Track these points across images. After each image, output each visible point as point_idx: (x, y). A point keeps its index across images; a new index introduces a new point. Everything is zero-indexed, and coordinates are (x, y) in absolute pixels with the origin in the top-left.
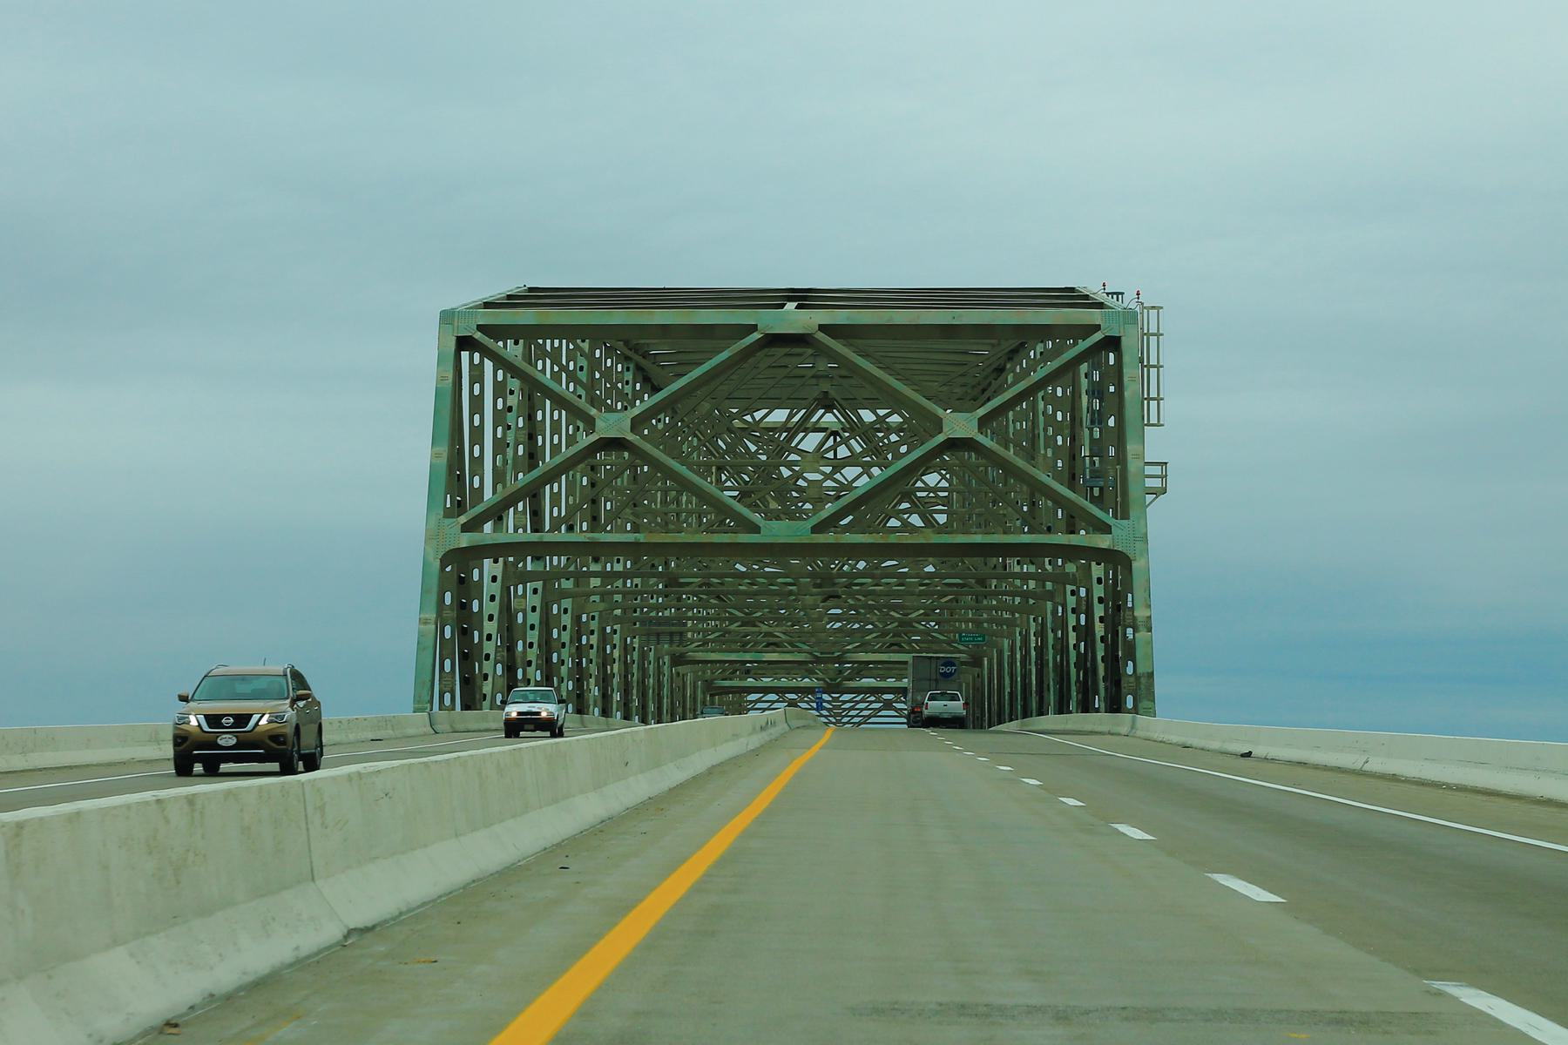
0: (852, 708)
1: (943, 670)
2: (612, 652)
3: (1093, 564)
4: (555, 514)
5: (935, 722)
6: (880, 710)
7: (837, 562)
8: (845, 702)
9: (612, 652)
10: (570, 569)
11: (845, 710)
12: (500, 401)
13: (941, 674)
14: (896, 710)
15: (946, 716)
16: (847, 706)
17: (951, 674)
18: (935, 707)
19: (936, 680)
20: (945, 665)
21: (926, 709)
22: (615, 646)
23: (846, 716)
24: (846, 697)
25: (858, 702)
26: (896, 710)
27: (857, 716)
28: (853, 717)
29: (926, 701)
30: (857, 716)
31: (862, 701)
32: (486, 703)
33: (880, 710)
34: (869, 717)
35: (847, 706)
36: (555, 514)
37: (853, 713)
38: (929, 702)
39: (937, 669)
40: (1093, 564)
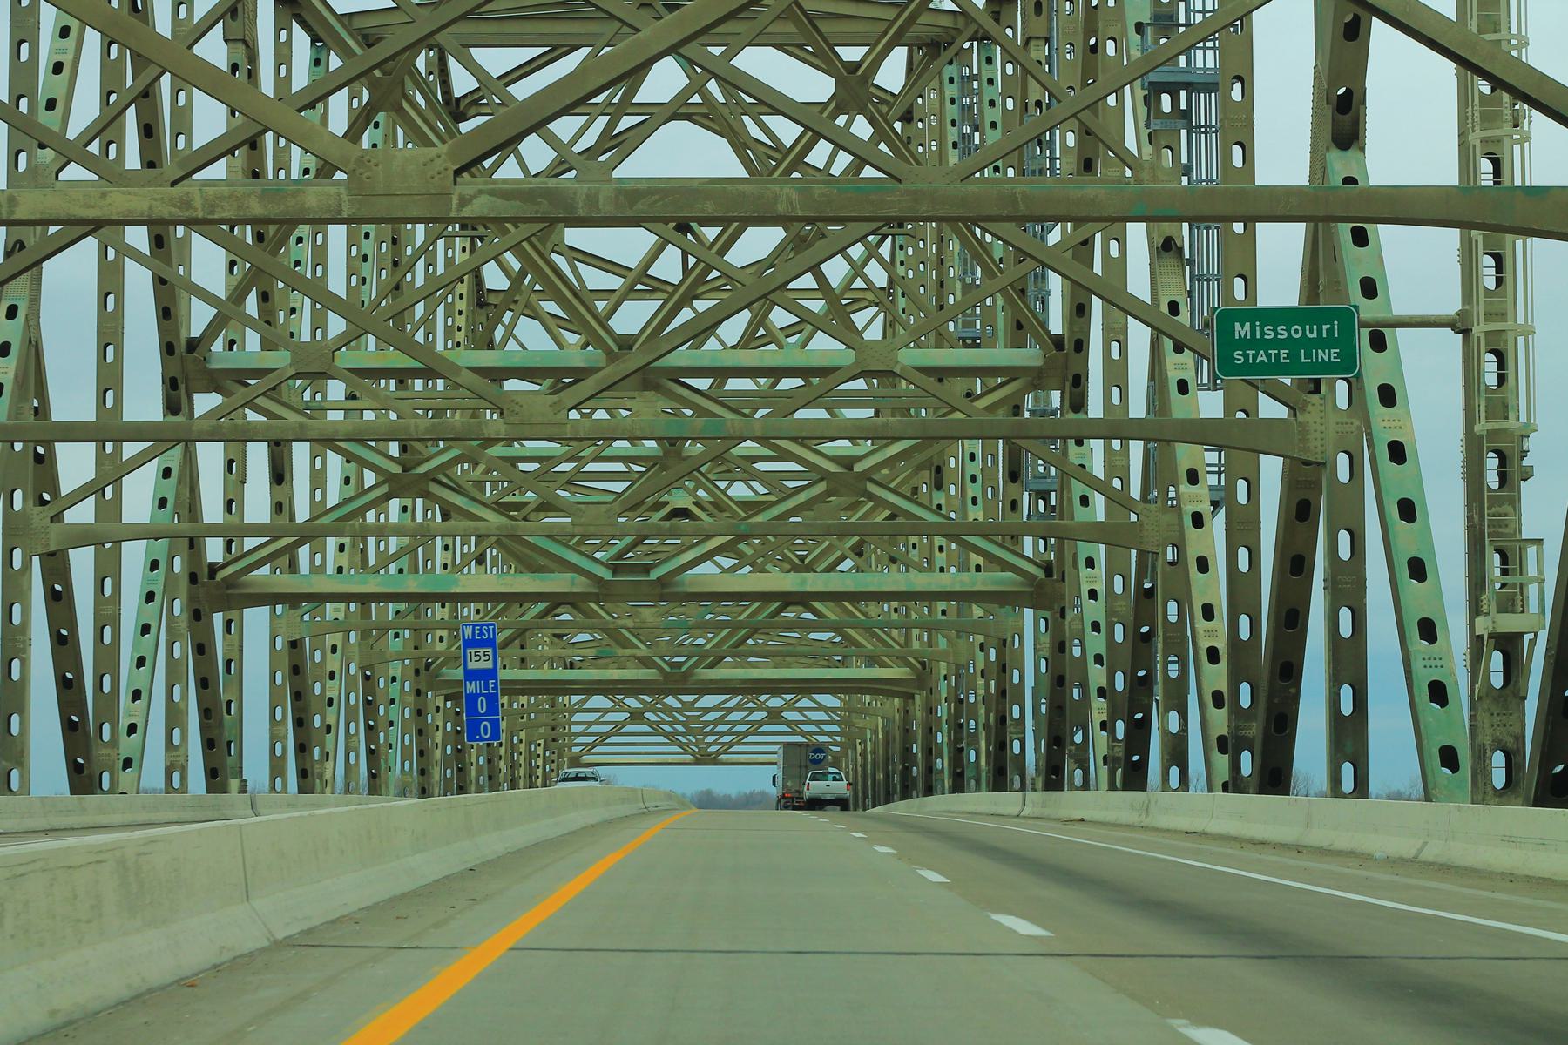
0: (717, 722)
1: (813, 756)
2: (518, 758)
3: (981, 519)
4: (466, 551)
5: (816, 804)
6: (762, 723)
7: (710, 635)
8: (706, 711)
9: (518, 758)
10: (247, 268)
11: (707, 724)
12: (354, 249)
13: (811, 761)
14: (788, 723)
15: (828, 797)
16: (712, 716)
17: (820, 761)
18: (816, 788)
19: (806, 767)
20: (815, 752)
21: (808, 789)
22: (538, 777)
23: (711, 733)
24: (709, 701)
25: (730, 710)
26: (788, 723)
27: (728, 733)
28: (721, 734)
29: (807, 781)
30: (728, 733)
31: (737, 709)
32: (328, 789)
33: (762, 723)
34: (746, 734)
35: (712, 716)
36: (466, 551)
37: (722, 728)
38: (811, 782)
39: (807, 756)
40: (981, 519)
